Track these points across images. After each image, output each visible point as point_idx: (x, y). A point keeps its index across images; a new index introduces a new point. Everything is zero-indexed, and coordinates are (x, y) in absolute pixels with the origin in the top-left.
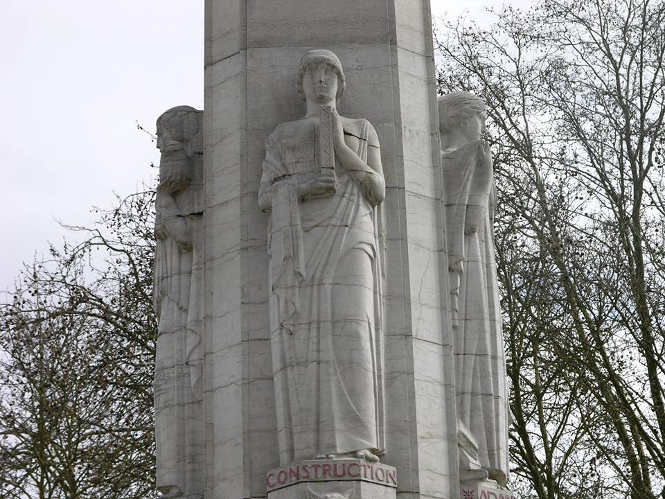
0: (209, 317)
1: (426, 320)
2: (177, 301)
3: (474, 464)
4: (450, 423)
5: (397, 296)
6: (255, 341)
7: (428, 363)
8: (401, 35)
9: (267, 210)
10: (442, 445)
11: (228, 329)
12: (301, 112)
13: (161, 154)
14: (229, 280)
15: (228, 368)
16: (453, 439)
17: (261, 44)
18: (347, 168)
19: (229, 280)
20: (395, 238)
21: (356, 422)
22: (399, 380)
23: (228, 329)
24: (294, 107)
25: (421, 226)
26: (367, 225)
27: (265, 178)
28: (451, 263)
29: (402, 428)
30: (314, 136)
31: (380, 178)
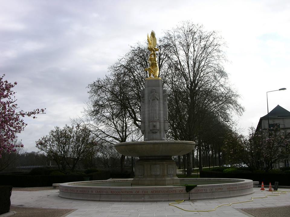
0: (145, 108)
1: (162, 109)
2: (67, 164)
3: (165, 120)
4: (163, 116)
5: (159, 107)
6: (149, 111)
7: (162, 112)
8: (160, 86)
9: (150, 101)
10: (163, 119)
11: (147, 109)
12: (152, 93)
13: (279, 189)
14: (147, 105)
15: (147, 112)
16: (164, 118)
17: (149, 87)
18: (156, 97)
19: (147, 105)
20: (159, 103)
21: (156, 118)
22: (159, 114)
23: (147, 109)
24: (152, 92)
25: (161, 101)
26: (157, 102)
27: (149, 98)
28: (164, 104)
29: (159, 117)
30: (153, 95)
31: (158, 98)
